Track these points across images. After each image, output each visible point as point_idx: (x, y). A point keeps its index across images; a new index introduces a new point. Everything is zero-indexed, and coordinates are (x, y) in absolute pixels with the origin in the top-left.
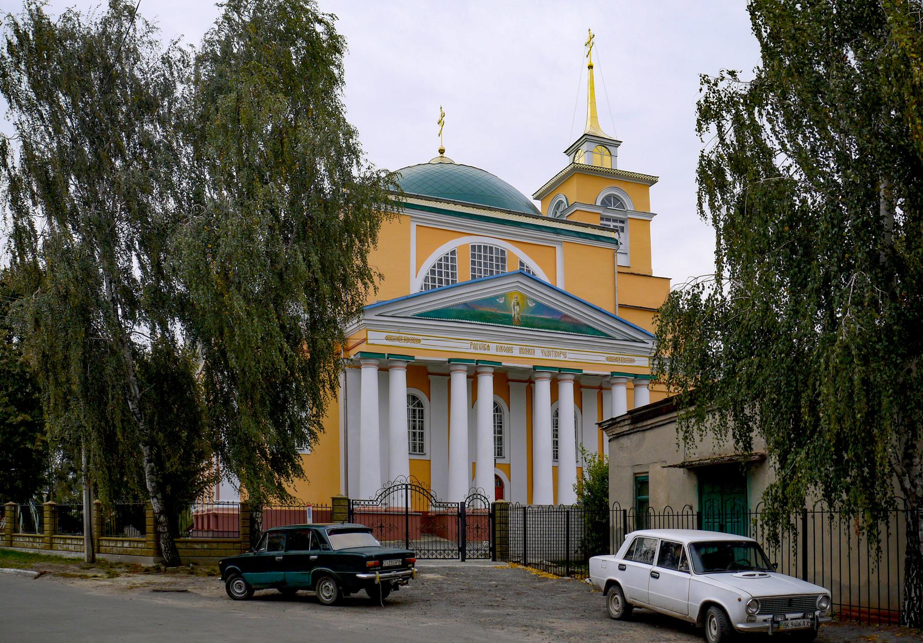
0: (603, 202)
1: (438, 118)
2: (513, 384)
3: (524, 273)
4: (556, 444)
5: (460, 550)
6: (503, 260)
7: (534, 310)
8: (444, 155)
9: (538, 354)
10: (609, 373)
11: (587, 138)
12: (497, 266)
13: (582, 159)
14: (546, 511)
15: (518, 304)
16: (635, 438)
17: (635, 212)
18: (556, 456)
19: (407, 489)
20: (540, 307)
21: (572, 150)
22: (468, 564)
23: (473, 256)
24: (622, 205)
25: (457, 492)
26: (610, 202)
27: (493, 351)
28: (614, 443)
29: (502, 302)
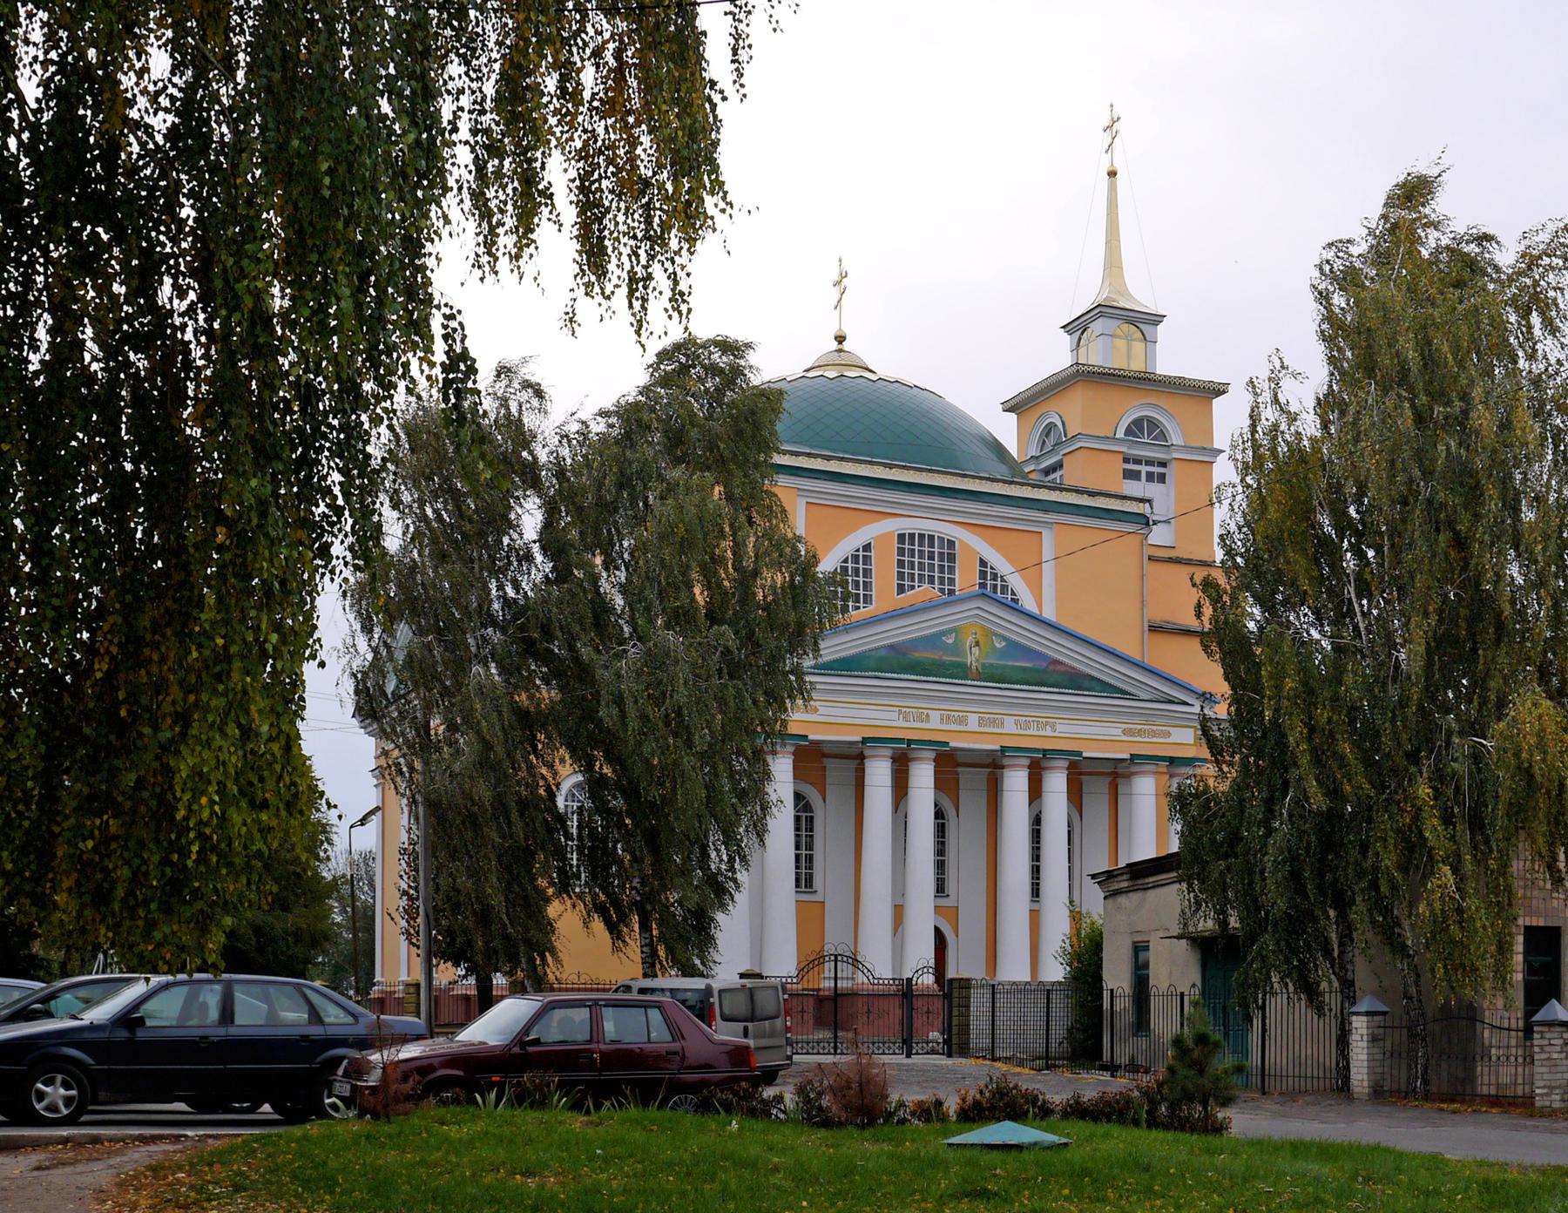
0: (1128, 432)
1: (836, 278)
2: (968, 775)
3: (991, 586)
4: (1036, 871)
5: (904, 1042)
6: (952, 558)
7: (1003, 653)
8: (846, 346)
9: (1010, 726)
10: (1126, 756)
11: (1102, 310)
12: (941, 568)
13: (1097, 355)
14: (1018, 989)
15: (977, 644)
16: (1135, 896)
17: (1187, 448)
18: (1036, 892)
19: (836, 961)
20: (1014, 648)
21: (1077, 327)
22: (915, 1059)
23: (901, 552)
24: (1163, 436)
25: (880, 962)
26: (1142, 431)
27: (935, 721)
28: (1110, 901)
29: (950, 641)
